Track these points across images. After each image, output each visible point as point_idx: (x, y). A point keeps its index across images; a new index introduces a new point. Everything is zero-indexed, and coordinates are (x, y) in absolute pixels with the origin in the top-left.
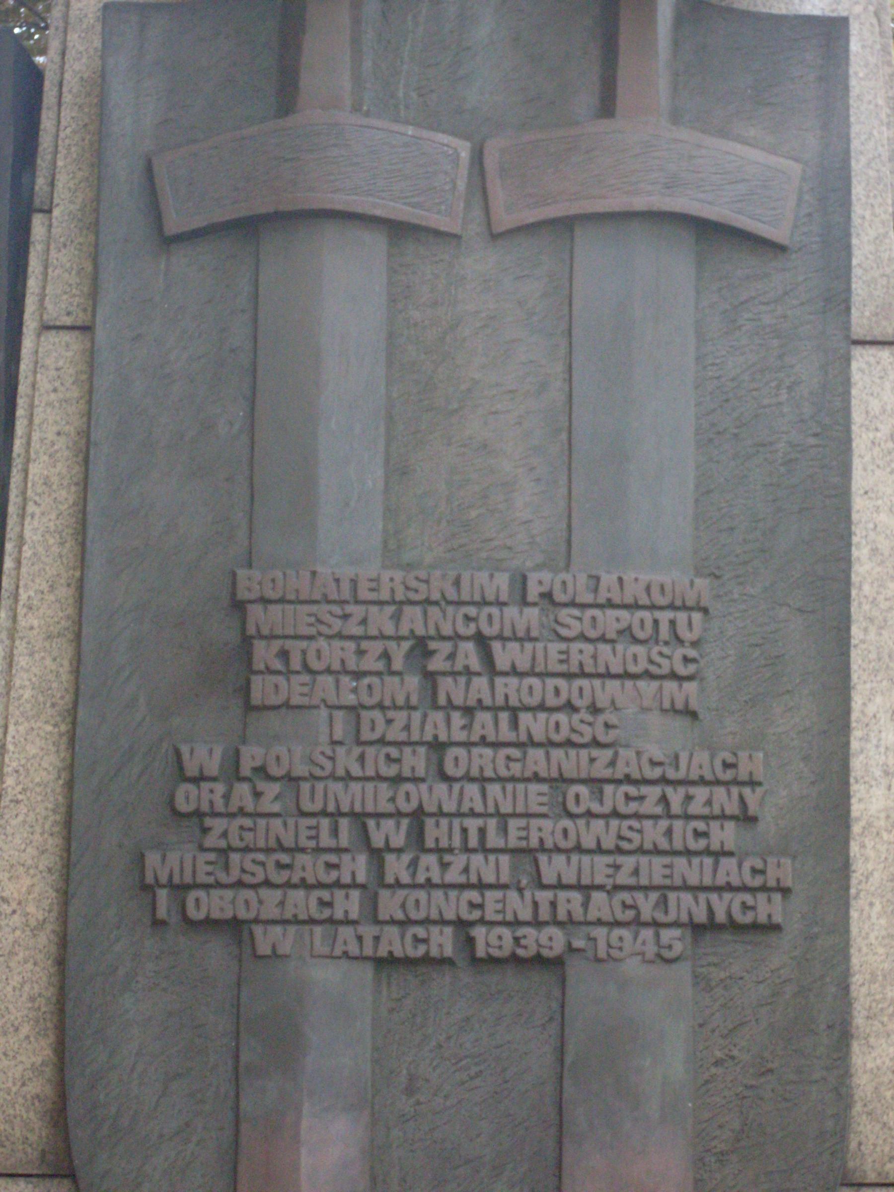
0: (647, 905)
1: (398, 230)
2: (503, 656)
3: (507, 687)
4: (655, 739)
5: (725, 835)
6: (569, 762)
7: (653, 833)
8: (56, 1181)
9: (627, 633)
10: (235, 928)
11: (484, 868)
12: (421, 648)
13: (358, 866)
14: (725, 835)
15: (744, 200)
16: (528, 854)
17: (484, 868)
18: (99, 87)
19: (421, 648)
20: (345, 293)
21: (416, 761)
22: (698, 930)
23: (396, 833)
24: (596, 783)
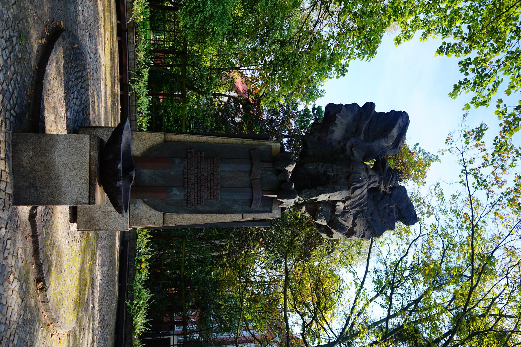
0: (189, 195)
1: (251, 172)
2: (212, 181)
3: (209, 182)
4: (205, 196)
5: (196, 202)
6: (202, 187)
7: (196, 195)
8: (88, 173)
9: (214, 193)
10: (187, 157)
11: (193, 180)
12: (212, 174)
13: (193, 168)
14: (196, 202)
15: (352, 312)
16: (194, 184)
17: (193, 180)
18: (265, 145)
19: (212, 174)
20: (246, 167)
21: (202, 174)
22: (187, 200)
23: (196, 171)
24: (200, 190)
